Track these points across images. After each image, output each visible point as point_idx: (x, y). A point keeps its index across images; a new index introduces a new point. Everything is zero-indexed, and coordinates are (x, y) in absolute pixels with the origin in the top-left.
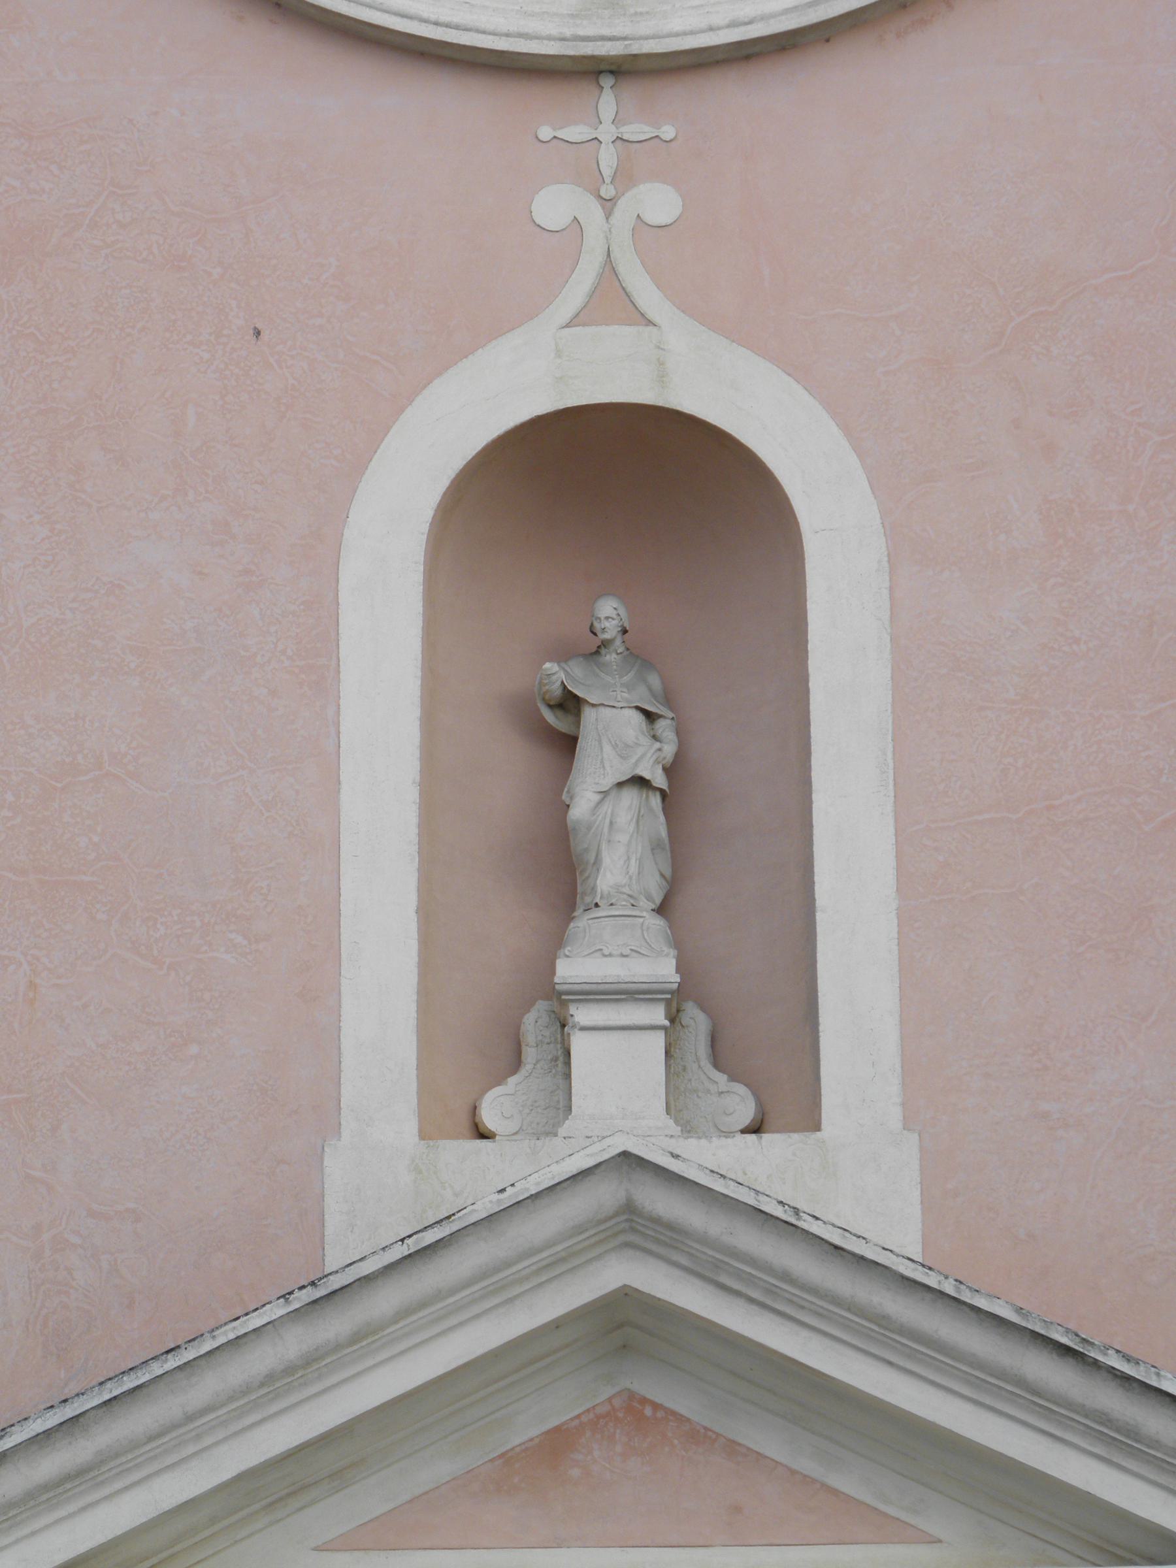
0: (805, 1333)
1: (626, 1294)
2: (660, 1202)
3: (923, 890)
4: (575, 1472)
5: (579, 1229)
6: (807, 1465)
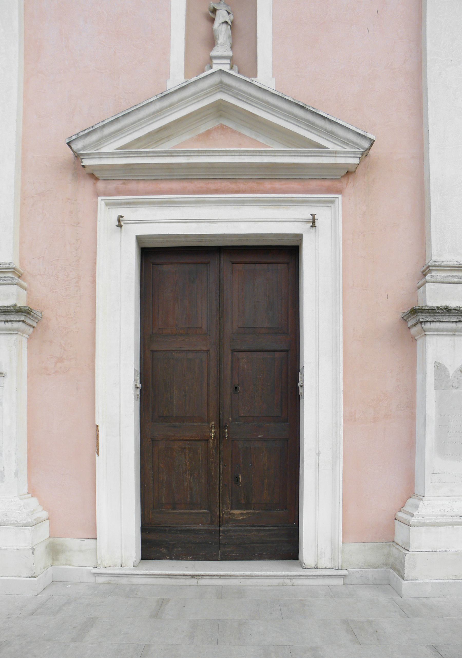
0: (253, 107)
1: (221, 100)
2: (227, 80)
3: (277, 35)
4: (211, 138)
5: (211, 86)
6: (253, 137)
